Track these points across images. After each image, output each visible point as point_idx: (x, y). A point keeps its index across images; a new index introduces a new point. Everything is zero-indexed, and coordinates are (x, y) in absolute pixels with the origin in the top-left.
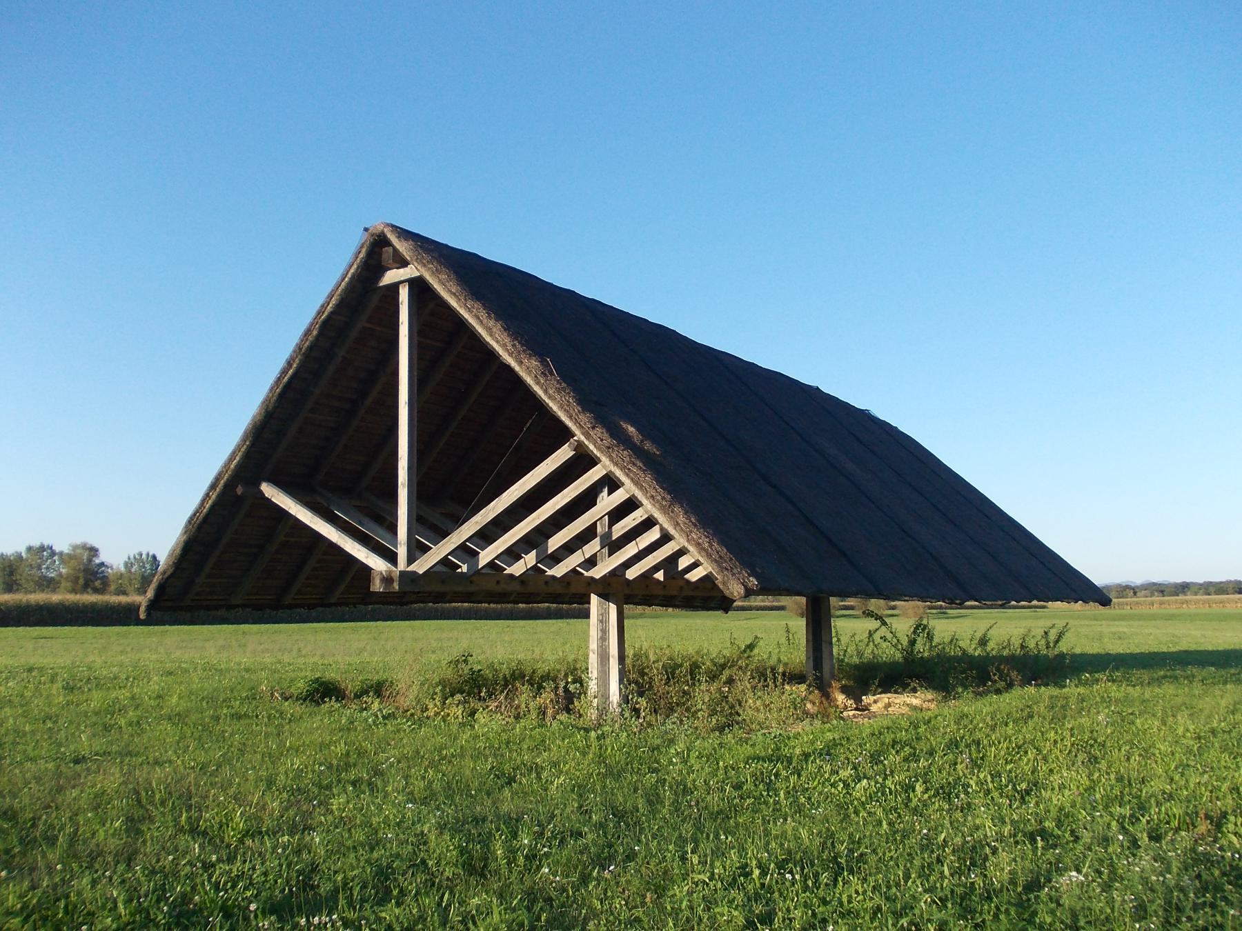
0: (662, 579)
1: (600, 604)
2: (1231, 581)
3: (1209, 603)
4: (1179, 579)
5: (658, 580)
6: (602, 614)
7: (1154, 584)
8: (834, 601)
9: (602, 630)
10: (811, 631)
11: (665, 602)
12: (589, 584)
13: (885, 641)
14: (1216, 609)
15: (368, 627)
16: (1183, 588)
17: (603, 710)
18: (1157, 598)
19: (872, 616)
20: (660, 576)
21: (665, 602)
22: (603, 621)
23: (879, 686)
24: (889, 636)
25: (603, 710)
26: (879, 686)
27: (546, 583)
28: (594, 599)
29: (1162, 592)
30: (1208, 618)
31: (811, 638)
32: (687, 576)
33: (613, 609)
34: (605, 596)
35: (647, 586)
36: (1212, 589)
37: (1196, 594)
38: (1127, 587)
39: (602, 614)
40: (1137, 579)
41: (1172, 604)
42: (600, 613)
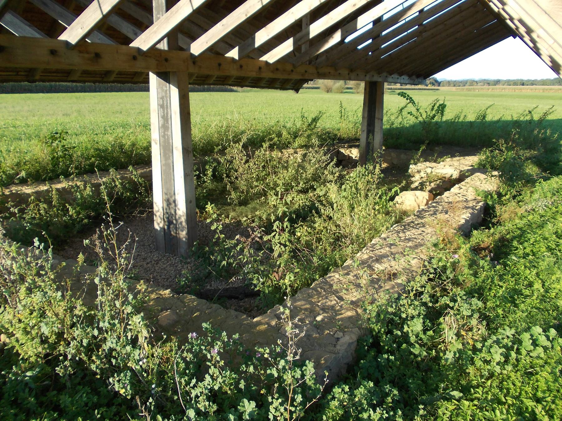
0: (237, 57)
1: (159, 86)
2: (531, 80)
3: (515, 90)
4: (496, 78)
5: (233, 59)
6: (162, 98)
7: (485, 80)
8: (386, 86)
9: (163, 117)
10: (367, 109)
11: (253, 84)
12: (135, 58)
13: (411, 115)
14: (517, 92)
15: (51, 98)
16: (497, 82)
17: (170, 219)
18: (486, 87)
19: (405, 97)
20: (234, 54)
21: (253, 84)
22: (164, 106)
23: (421, 156)
24: (414, 112)
25: (170, 219)
26: (421, 156)
27: (53, 52)
28: (153, 78)
29: (489, 84)
30: (519, 97)
31: (366, 115)
32: (264, 58)
33: (174, 92)
34: (164, 76)
35: (220, 65)
36: (512, 83)
37: (503, 85)
38: (474, 81)
39: (162, 98)
40: (477, 78)
41: (490, 90)
42: (160, 96)
